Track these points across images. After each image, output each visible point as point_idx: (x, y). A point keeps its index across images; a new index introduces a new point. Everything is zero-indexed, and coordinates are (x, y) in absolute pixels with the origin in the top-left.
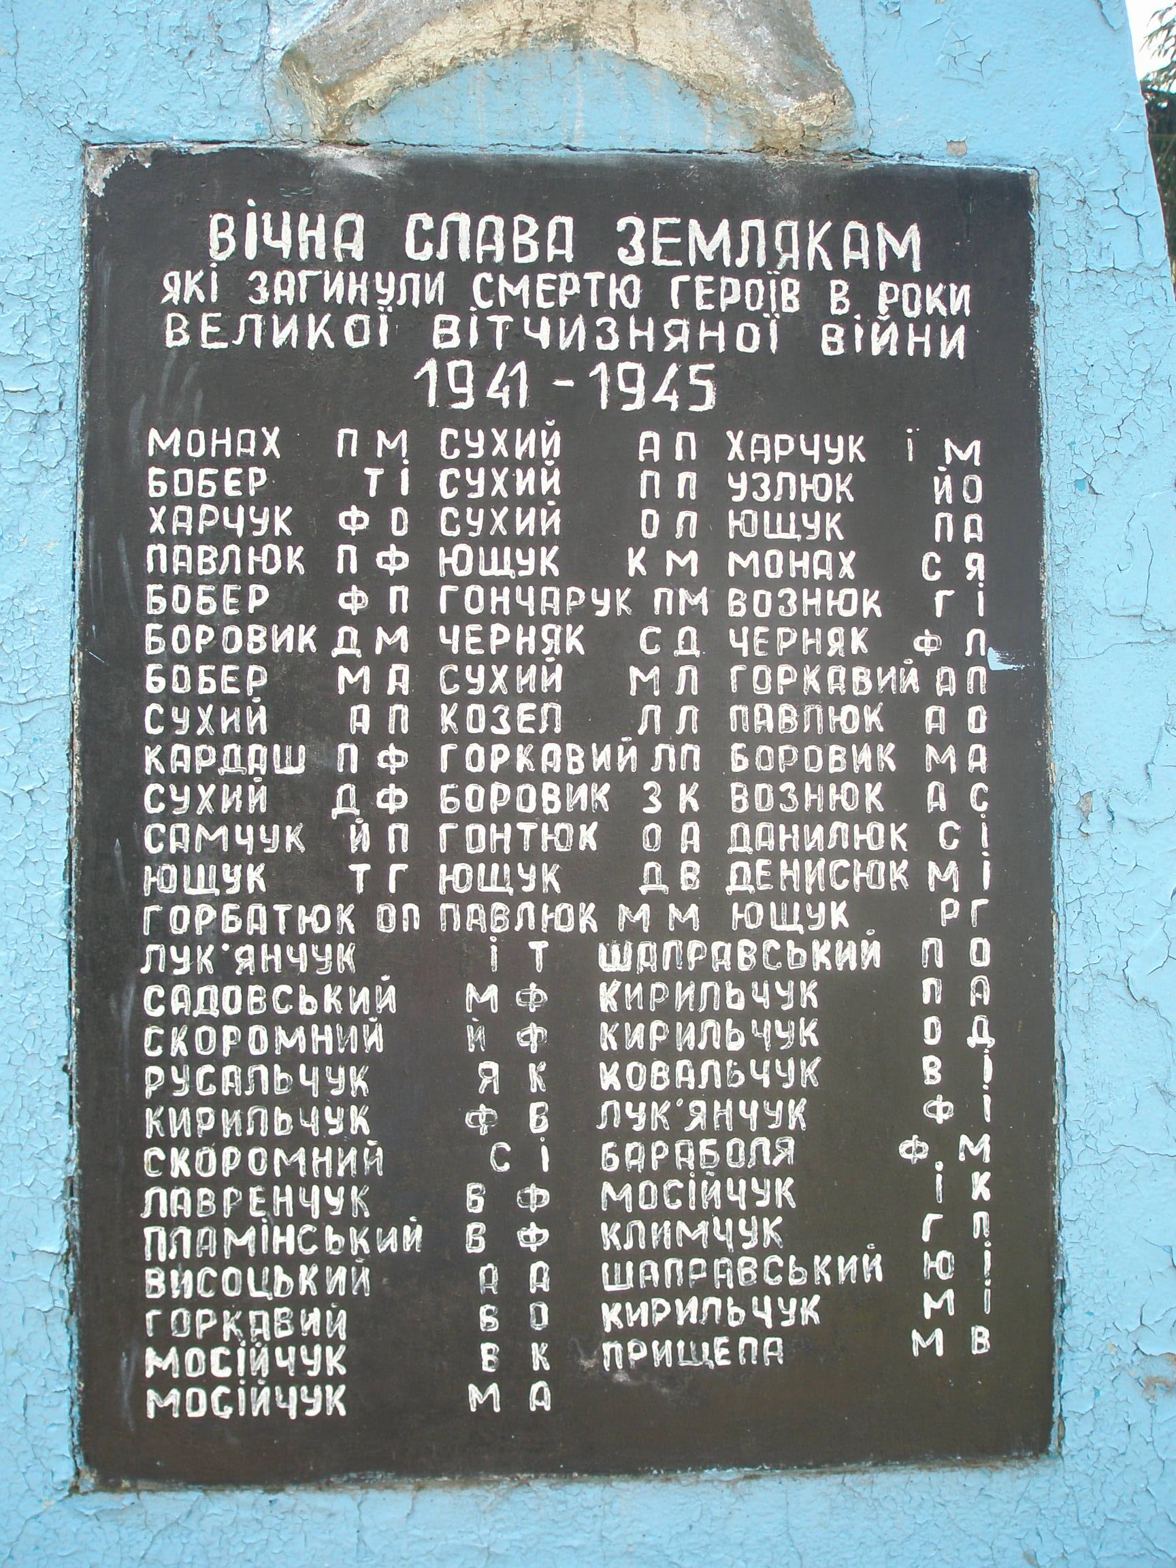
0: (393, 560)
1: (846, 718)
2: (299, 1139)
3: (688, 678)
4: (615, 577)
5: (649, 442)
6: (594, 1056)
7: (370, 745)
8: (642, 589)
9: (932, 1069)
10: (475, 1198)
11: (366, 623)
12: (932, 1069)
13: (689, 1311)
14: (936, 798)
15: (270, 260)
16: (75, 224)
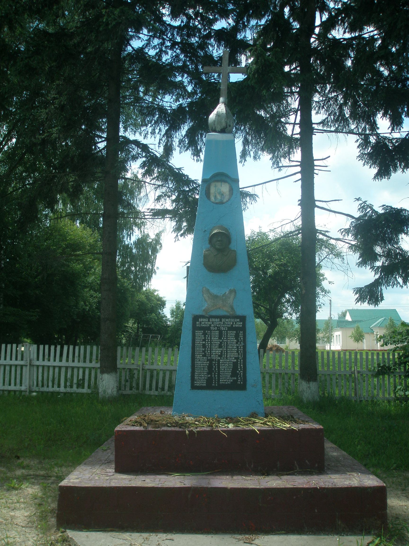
0: (209, 338)
1: (234, 347)
2: (203, 370)
3: (225, 345)
4: (221, 339)
5: (223, 332)
6: (220, 366)
7: (208, 348)
8: (223, 340)
9: (239, 367)
10: (213, 374)
11: (208, 342)
12: (239, 367)
13: (225, 380)
14: (239, 352)
15: (202, 321)
16: (191, 319)
